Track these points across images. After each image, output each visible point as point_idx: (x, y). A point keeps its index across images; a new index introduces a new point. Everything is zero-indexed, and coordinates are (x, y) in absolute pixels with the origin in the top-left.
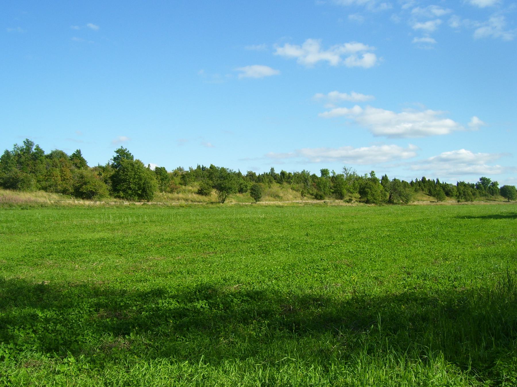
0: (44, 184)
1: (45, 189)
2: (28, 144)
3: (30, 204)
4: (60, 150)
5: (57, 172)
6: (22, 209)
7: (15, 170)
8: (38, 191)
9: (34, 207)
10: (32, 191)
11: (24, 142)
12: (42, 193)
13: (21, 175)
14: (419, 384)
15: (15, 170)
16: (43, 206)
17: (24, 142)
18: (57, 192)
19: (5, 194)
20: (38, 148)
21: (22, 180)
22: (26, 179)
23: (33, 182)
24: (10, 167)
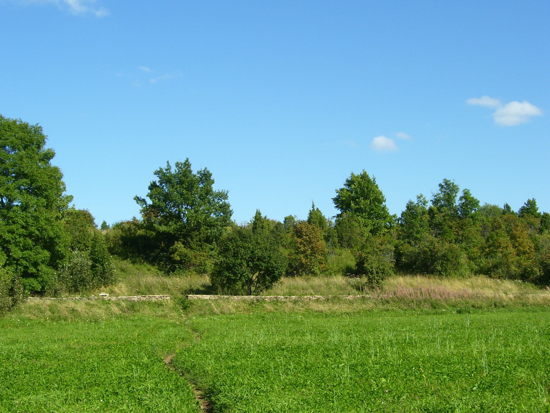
0: (484, 262)
1: (487, 272)
2: (448, 189)
3: (473, 302)
4: (380, 188)
5: (504, 240)
6: (459, 312)
7: (428, 238)
8: (474, 278)
9: (480, 308)
10: (462, 276)
11: (440, 185)
12: (481, 280)
13: (442, 247)
14: (171, 411)
15: (428, 238)
16: (497, 305)
17: (440, 185)
18: (512, 277)
19: (415, 284)
20: (466, 196)
21: (444, 256)
22: (450, 256)
23: (463, 259)
24: (418, 232)
